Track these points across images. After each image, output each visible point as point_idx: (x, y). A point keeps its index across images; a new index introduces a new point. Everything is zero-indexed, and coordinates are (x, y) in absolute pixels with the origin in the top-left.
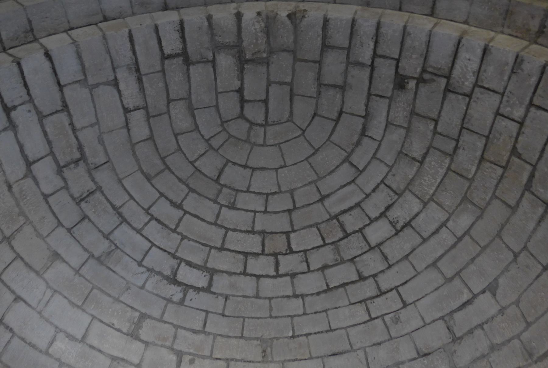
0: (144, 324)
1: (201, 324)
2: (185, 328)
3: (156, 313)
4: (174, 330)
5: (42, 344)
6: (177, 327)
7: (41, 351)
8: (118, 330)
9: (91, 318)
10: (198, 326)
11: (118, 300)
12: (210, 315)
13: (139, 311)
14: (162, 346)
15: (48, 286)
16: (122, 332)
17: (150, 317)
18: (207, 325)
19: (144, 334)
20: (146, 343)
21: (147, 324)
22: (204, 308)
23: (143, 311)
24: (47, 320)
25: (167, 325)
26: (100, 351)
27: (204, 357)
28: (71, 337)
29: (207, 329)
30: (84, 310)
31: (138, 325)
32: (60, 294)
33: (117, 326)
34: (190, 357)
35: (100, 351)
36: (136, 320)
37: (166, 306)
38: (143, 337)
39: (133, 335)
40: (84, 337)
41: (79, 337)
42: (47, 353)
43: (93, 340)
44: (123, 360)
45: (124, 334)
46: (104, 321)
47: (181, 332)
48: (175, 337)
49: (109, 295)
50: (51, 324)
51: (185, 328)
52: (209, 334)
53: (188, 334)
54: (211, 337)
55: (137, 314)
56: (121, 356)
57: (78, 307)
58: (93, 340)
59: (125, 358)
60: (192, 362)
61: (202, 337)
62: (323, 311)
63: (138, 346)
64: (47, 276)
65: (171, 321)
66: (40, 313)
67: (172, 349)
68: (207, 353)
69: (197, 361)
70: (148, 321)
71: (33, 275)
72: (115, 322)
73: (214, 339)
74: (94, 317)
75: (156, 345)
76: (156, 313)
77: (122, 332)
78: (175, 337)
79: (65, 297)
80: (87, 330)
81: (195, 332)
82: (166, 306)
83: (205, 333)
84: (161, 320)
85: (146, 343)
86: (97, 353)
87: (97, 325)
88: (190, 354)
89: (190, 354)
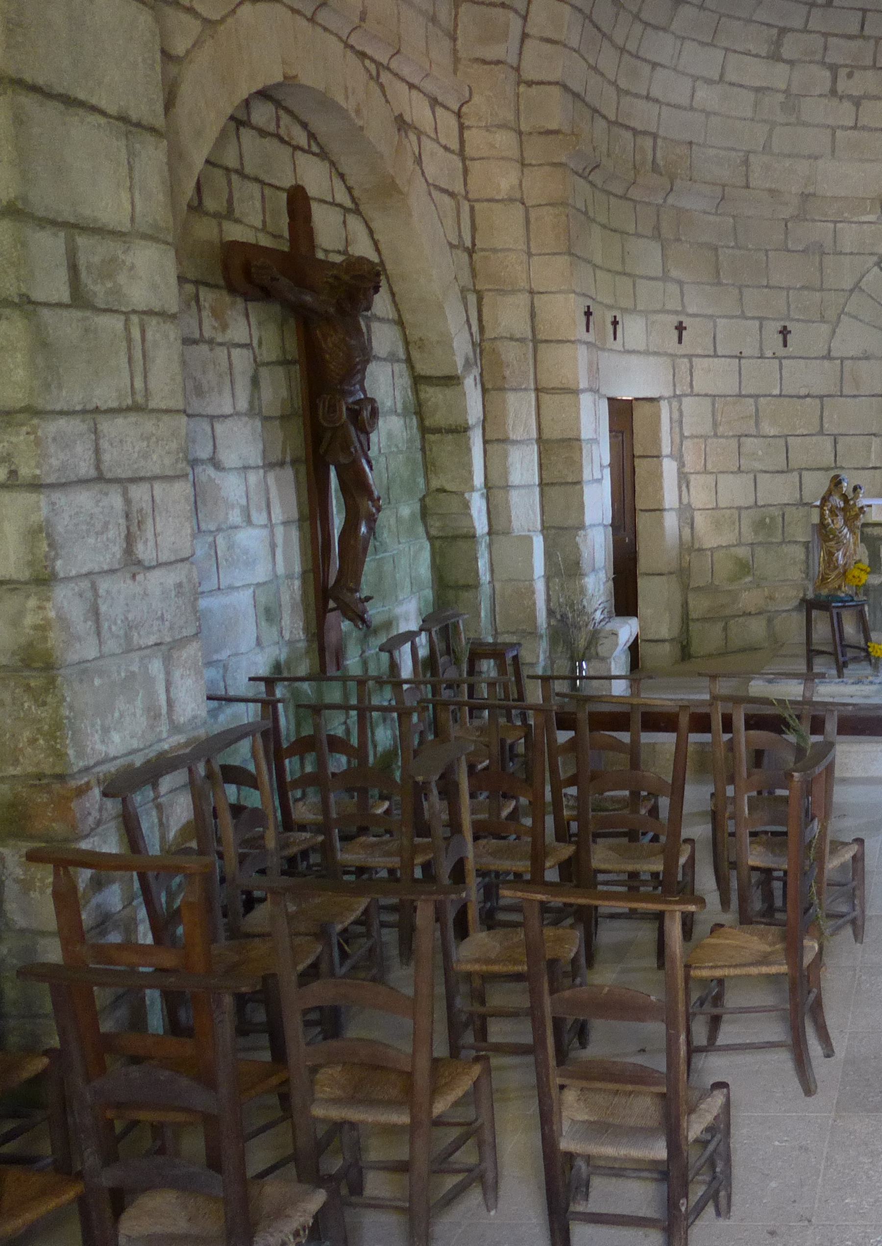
0: (785, 40)
1: (858, 27)
2: (836, 35)
3: (798, 23)
4: (823, 39)
5: (685, 101)
6: (825, 35)
7: (685, 109)
8: (756, 56)
9: (724, 52)
10: (854, 29)
11: (750, 21)
12: (869, 14)
13: (777, 27)
14: (811, 62)
15: (677, 37)
16: (760, 56)
17: (792, 30)
18: (866, 27)
19: (786, 52)
20: (791, 63)
21: (789, 38)
22: (859, 5)
23: (781, 24)
24: (683, 74)
25: (813, 36)
26: (741, 86)
27: (865, 68)
28: (709, 82)
29: (867, 32)
30: (715, 46)
31: (778, 44)
32: (688, 38)
33: (754, 52)
34: (848, 70)
35: (741, 86)
36: (775, 38)
37: (809, 12)
38: (785, 56)
39: (775, 57)
40: (722, 76)
41: (717, 78)
42: (692, 108)
43: (731, 76)
44: (768, 88)
45: (764, 58)
46: (738, 49)
47: (832, 41)
48: (825, 49)
49: (739, 19)
50: (687, 75)
51: (836, 35)
52: (869, 38)
53: (842, 42)
54: (872, 42)
55: (775, 31)
56: (764, 85)
57: (707, 44)
58: (731, 76)
59: (770, 85)
60: (850, 75)
61: (860, 42)
62: (817, 397)
63: (782, 69)
64: (673, 28)
65: (818, 29)
66: (675, 69)
67: (823, 63)
68: (868, 62)
69: (857, 74)
70: (789, 34)
71: (661, 33)
72: (751, 47)
73: (877, 43)
74: (727, 49)
75: (804, 62)
76: (798, 23)
77: (760, 56)
78: (825, 49)
79: (694, 40)
80: (723, 67)
81: (850, 37)
82: (809, 12)
83: (864, 38)
84: (805, 30)
85: (791, 63)
86: (739, 89)
87: (732, 57)
88: (846, 66)
89: (846, 66)
